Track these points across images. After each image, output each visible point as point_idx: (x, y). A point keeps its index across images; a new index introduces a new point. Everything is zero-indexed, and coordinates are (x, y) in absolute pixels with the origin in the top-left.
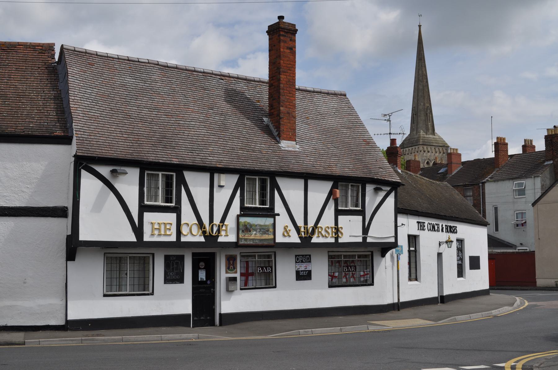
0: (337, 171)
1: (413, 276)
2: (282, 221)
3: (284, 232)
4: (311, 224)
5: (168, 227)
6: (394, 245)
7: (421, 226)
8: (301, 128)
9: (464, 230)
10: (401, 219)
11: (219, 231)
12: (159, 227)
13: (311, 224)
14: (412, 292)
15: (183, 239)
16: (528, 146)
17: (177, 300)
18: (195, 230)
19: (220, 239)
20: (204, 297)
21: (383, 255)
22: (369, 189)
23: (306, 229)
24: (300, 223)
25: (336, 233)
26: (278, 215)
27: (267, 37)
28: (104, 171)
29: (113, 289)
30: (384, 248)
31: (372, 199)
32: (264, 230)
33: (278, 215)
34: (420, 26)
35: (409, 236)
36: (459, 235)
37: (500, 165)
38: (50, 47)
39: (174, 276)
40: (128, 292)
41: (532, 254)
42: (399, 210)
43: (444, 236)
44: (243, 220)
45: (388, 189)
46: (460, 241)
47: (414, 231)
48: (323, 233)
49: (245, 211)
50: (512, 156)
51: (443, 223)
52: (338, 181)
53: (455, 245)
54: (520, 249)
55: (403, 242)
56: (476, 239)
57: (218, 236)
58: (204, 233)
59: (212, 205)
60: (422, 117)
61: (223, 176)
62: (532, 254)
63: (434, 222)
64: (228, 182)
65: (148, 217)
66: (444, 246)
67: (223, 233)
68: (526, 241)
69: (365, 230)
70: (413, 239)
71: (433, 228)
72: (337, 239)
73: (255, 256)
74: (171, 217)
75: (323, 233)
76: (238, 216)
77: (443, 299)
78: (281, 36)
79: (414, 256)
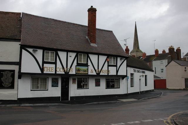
0: (108, 53)
1: (132, 86)
2: (91, 68)
3: (91, 71)
4: (100, 69)
5: (52, 69)
6: (126, 76)
7: (135, 71)
8: (97, 39)
9: (147, 73)
10: (128, 68)
11: (69, 70)
12: (49, 69)
13: (100, 69)
14: (131, 90)
15: (57, 73)
16: (164, 52)
17: (56, 92)
18: (62, 70)
19: (70, 73)
20: (65, 91)
21: (123, 79)
22: (119, 59)
23: (98, 71)
24: (96, 68)
25: (108, 72)
26: (89, 66)
27: (87, 12)
28: (31, 50)
29: (35, 88)
30: (123, 77)
31: (119, 62)
32: (85, 71)
33: (89, 66)
34: (136, 22)
35: (131, 74)
36: (146, 74)
37: (158, 56)
38: (20, 14)
39: (55, 84)
40: (39, 89)
41: (165, 80)
42: (128, 66)
43: (141, 74)
44: (77, 67)
45: (125, 59)
46: (146, 76)
47: (133, 72)
48: (104, 72)
49: (78, 64)
50: (159, 54)
51: (141, 70)
52: (109, 56)
53: (144, 76)
54: (162, 78)
55: (129, 75)
56: (150, 76)
57: (69, 72)
58: (64, 71)
59: (67, 62)
60: (136, 44)
61: (71, 53)
62: (165, 80)
63: (138, 70)
64: (73, 55)
65: (45, 65)
66: (142, 77)
67: (71, 71)
68: (162, 76)
69: (117, 72)
70: (132, 75)
71: (138, 72)
72: (108, 74)
73: (82, 79)
74: (54, 66)
75: (104, 72)
76: (76, 66)
77: (142, 93)
78: (92, 12)
79: (132, 79)
